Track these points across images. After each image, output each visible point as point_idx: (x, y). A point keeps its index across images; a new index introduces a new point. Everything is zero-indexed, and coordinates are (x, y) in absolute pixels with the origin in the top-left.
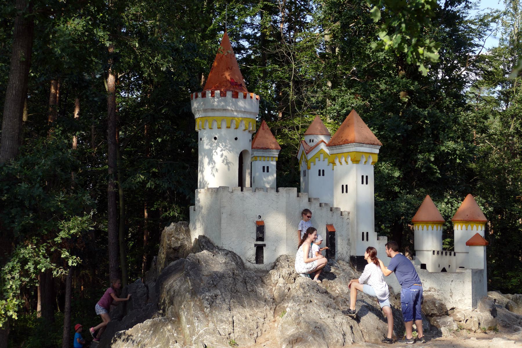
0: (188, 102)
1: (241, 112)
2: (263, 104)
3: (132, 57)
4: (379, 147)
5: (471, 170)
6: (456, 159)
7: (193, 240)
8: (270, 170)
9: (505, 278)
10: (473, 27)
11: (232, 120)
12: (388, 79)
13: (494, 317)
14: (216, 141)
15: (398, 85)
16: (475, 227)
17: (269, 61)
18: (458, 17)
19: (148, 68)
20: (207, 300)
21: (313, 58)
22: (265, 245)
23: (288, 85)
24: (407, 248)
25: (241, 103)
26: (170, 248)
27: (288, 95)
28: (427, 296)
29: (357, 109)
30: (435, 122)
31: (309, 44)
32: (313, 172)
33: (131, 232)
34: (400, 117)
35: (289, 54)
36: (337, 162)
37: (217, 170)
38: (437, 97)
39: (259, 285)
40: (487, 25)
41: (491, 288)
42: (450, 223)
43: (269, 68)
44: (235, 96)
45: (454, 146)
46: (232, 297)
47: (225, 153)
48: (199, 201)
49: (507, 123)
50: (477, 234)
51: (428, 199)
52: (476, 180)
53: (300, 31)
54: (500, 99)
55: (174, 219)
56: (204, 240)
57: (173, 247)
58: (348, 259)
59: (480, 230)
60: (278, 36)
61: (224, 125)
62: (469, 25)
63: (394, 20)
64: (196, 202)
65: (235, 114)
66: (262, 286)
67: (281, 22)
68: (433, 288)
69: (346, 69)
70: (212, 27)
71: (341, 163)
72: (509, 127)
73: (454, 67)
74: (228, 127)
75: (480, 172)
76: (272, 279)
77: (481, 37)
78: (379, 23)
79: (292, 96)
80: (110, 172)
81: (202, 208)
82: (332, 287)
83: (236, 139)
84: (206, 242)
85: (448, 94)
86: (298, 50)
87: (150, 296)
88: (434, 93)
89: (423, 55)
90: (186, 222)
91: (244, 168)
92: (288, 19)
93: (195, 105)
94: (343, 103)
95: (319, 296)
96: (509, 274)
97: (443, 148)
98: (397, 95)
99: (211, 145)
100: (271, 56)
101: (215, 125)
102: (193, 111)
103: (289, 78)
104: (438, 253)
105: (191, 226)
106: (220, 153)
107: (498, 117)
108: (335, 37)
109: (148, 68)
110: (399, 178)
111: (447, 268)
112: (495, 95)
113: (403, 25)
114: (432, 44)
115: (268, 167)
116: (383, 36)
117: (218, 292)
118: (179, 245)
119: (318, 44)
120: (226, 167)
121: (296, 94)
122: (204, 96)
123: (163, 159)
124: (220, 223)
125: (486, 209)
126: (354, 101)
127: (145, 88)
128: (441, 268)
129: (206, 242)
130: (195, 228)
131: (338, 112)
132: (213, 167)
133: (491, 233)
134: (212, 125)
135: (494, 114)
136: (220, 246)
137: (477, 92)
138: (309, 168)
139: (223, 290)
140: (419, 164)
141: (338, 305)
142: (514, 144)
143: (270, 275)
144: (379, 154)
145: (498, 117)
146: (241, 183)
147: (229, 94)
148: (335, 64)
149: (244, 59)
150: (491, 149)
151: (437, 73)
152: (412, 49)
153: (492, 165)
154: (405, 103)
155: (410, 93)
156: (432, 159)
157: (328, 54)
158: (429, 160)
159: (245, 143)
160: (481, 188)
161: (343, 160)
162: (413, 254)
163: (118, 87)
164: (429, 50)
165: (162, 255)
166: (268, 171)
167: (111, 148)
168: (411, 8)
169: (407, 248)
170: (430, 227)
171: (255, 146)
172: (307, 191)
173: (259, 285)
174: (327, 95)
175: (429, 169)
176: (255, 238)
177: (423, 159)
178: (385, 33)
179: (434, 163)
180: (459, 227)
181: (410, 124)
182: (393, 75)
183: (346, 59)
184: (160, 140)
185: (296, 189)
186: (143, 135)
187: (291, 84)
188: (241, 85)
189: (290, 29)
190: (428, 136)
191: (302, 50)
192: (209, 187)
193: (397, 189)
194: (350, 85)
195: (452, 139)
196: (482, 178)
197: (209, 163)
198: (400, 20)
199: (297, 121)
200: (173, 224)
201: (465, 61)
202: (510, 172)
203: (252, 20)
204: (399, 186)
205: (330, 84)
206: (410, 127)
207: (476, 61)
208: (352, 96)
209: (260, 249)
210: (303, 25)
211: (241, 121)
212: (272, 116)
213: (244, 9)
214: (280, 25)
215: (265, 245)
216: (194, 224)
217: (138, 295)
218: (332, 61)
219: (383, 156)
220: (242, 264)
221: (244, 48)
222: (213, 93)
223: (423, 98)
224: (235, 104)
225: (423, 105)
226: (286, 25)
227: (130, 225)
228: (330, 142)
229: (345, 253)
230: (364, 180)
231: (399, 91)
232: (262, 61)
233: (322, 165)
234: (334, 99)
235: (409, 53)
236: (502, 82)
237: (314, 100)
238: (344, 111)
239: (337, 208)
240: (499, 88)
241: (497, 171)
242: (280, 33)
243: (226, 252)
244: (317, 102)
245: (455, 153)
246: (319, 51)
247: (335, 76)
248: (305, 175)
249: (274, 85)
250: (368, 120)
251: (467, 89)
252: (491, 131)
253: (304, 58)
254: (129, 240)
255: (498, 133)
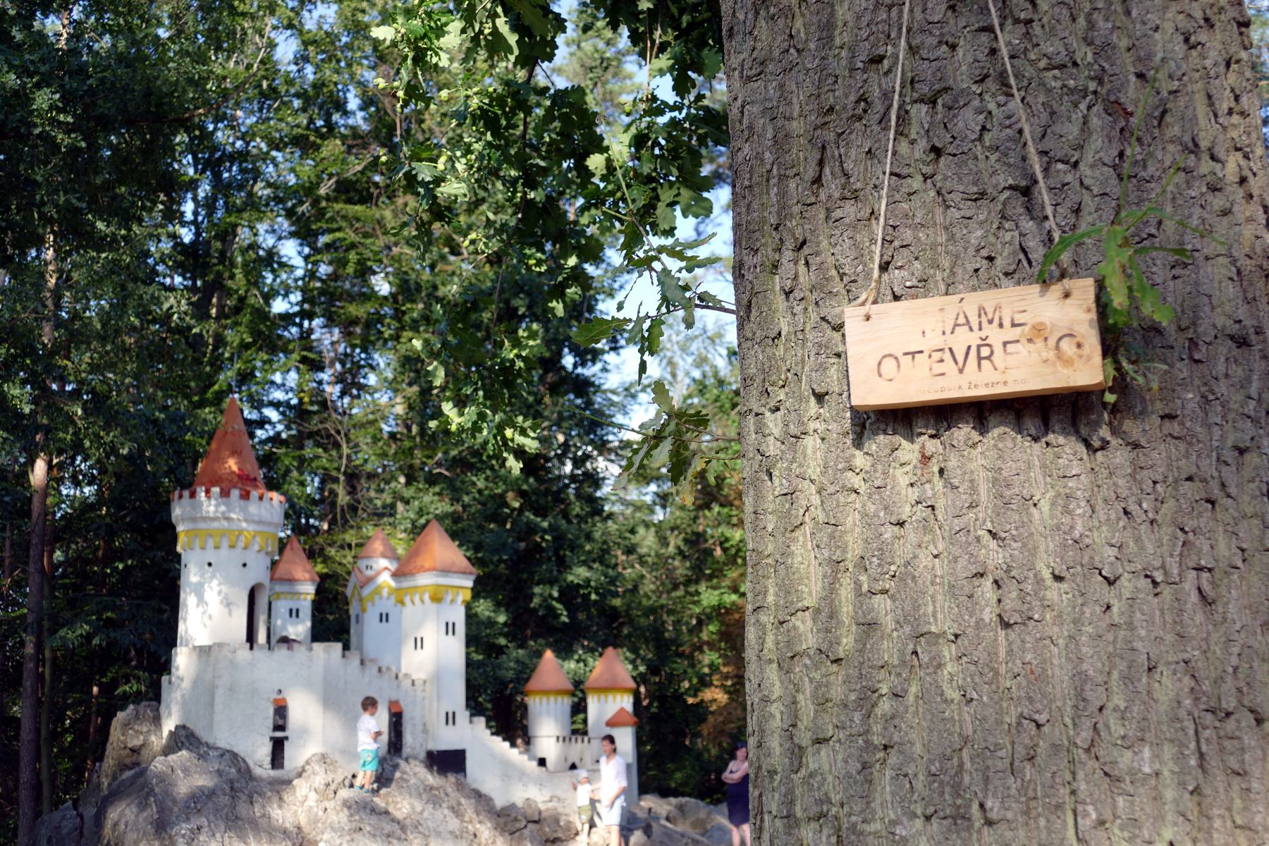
0: (166, 506)
1: (254, 522)
2: (293, 513)
3: (71, 430)
4: (473, 577)
5: (614, 608)
6: (590, 593)
7: (165, 733)
8: (301, 614)
9: (664, 772)
10: (615, 398)
11: (238, 537)
12: (488, 472)
13: (649, 837)
14: (211, 569)
15: (505, 482)
16: (618, 697)
17: (309, 443)
18: (592, 384)
19: (98, 449)
20: (183, 836)
21: (376, 439)
22: (287, 738)
23: (336, 480)
24: (520, 732)
25: (254, 508)
26: (125, 748)
27: (336, 495)
28: (547, 810)
29: (440, 518)
30: (559, 538)
31: (371, 417)
32: (370, 618)
33: (70, 718)
34: (508, 531)
35: (338, 432)
36: (407, 600)
37: (210, 617)
38: (563, 501)
39: (275, 806)
40: (634, 396)
41: (644, 789)
42: (583, 691)
43: (309, 451)
44: (245, 496)
45: (588, 574)
46: (228, 828)
47: (224, 588)
48: (177, 669)
49: (665, 538)
50: (622, 710)
51: (549, 654)
52: (622, 624)
53: (358, 397)
54: (654, 503)
55: (137, 698)
56: (183, 732)
57: (130, 745)
58: (423, 755)
59: (626, 702)
60: (324, 404)
61: (225, 544)
62: (610, 395)
63: (466, 385)
64: (173, 670)
65: (244, 525)
66: (280, 807)
67: (329, 383)
68: (865, 111)
69: (429, 457)
70: (216, 387)
71: (413, 602)
72: (668, 545)
73: (587, 457)
74: (232, 547)
75: (627, 611)
76: (298, 793)
77: (626, 413)
78: (443, 388)
79: (343, 498)
80: (30, 619)
81: (182, 680)
82: (397, 803)
83: (245, 565)
84: (187, 737)
85: (578, 495)
86: (354, 426)
87: (85, 831)
88: (559, 497)
89: (512, 440)
90: (154, 703)
91: (256, 612)
92: (340, 379)
93: (177, 511)
94: (421, 509)
95: (374, 819)
96: (671, 766)
97: (570, 578)
98: (502, 496)
99: (202, 576)
100: (311, 435)
101: (211, 543)
102: (174, 520)
103: (338, 469)
104: (564, 739)
105: (163, 708)
106: (216, 589)
107: (653, 529)
108: (410, 407)
109: (98, 449)
110: (505, 624)
111: (577, 763)
112: (648, 499)
113: (481, 393)
114: (528, 424)
115: (298, 611)
116: (448, 408)
117: (203, 821)
118: (141, 742)
119: (385, 418)
120: (226, 611)
121: (349, 493)
122: (193, 495)
123: (126, 597)
124: (212, 704)
125: (636, 668)
126: (439, 505)
127: (101, 481)
128: (569, 763)
129: (187, 737)
130: (170, 714)
131: (413, 522)
132: (204, 613)
133: (645, 703)
134: (205, 542)
135: (647, 525)
136: (211, 741)
137: (622, 494)
138: (364, 611)
139: (212, 818)
140: (536, 601)
141: (405, 833)
142: (675, 569)
143: (294, 787)
144: (472, 589)
145: (653, 529)
146: (251, 637)
147: (235, 493)
148: (411, 449)
149: (269, 439)
150: (643, 577)
151: (564, 464)
152: (495, 431)
153: (645, 602)
154: (514, 509)
155: (522, 494)
156: (556, 594)
157: (402, 434)
158: (550, 596)
159: (259, 572)
160: (629, 636)
161: (417, 599)
162: (528, 741)
163: (54, 479)
164: (523, 432)
165: (109, 762)
166: (297, 616)
167: (34, 579)
168: (493, 366)
169: (520, 732)
170: (552, 699)
171: (277, 575)
172: (360, 648)
173: (275, 806)
174: (398, 497)
175: (551, 610)
176: (271, 726)
177: (541, 595)
178: (450, 404)
179: (558, 600)
180: (596, 698)
181: (522, 540)
182: (497, 467)
183: (428, 442)
184: (121, 566)
185: (339, 646)
186: (96, 557)
187: (342, 478)
188: (255, 479)
189: (343, 393)
190: (549, 559)
191: (362, 425)
192: (197, 643)
193: (502, 641)
194: (432, 480)
195: (584, 563)
196: (631, 621)
197: (198, 605)
198: (476, 384)
199: (350, 537)
200: (131, 707)
201: (603, 447)
202: (671, 612)
203: (284, 379)
204: (506, 635)
205: (402, 480)
206: (523, 545)
207: (621, 448)
208: (436, 498)
209: (278, 746)
210: (361, 387)
211: (254, 537)
212: (313, 526)
213: (270, 362)
214: (328, 389)
215: (287, 738)
216: (168, 707)
217: (64, 831)
218: (407, 444)
219: (477, 592)
220: (249, 770)
221: (269, 422)
222: (207, 492)
223: (542, 501)
224: (244, 510)
225: (541, 512)
226: (338, 388)
227: (68, 707)
228: (397, 570)
229: (418, 745)
230: (450, 628)
231: (506, 492)
232: (297, 442)
233: (387, 605)
234: (407, 502)
235: (491, 437)
236: (657, 479)
237: (379, 503)
238: (423, 521)
239: (406, 675)
240: (653, 487)
241: (652, 610)
242: (325, 400)
243: (220, 752)
244: (384, 507)
245: (589, 586)
246: (386, 428)
247: (411, 467)
248: (357, 621)
249: (317, 480)
250: (456, 536)
251: (606, 490)
252: (643, 551)
253: (364, 440)
254: (66, 731)
255: (653, 554)
